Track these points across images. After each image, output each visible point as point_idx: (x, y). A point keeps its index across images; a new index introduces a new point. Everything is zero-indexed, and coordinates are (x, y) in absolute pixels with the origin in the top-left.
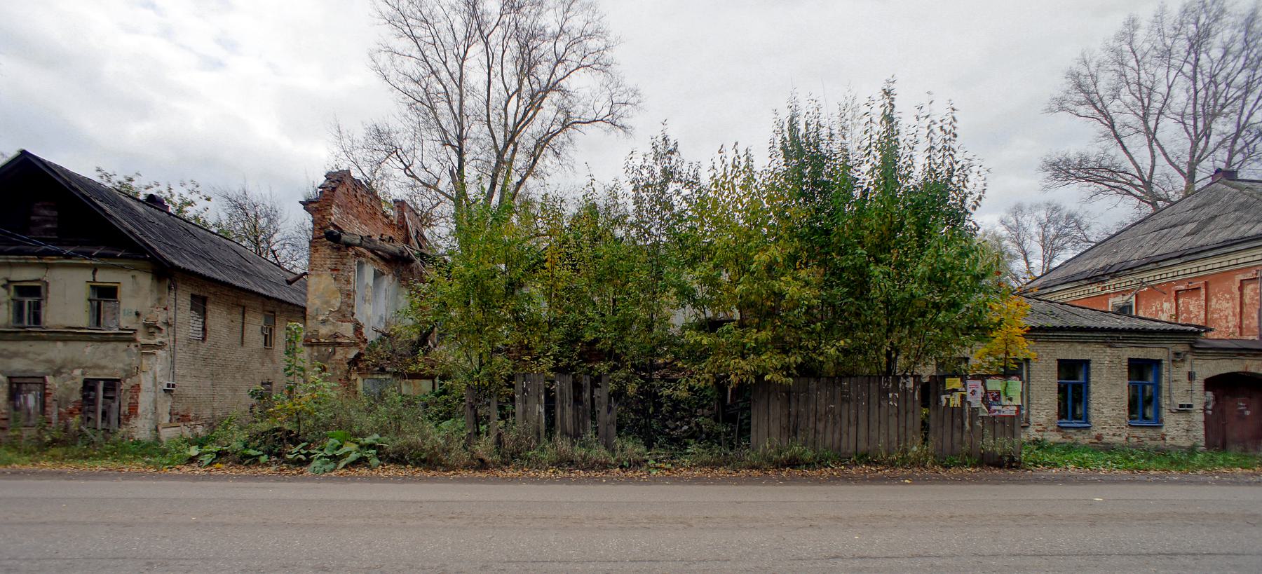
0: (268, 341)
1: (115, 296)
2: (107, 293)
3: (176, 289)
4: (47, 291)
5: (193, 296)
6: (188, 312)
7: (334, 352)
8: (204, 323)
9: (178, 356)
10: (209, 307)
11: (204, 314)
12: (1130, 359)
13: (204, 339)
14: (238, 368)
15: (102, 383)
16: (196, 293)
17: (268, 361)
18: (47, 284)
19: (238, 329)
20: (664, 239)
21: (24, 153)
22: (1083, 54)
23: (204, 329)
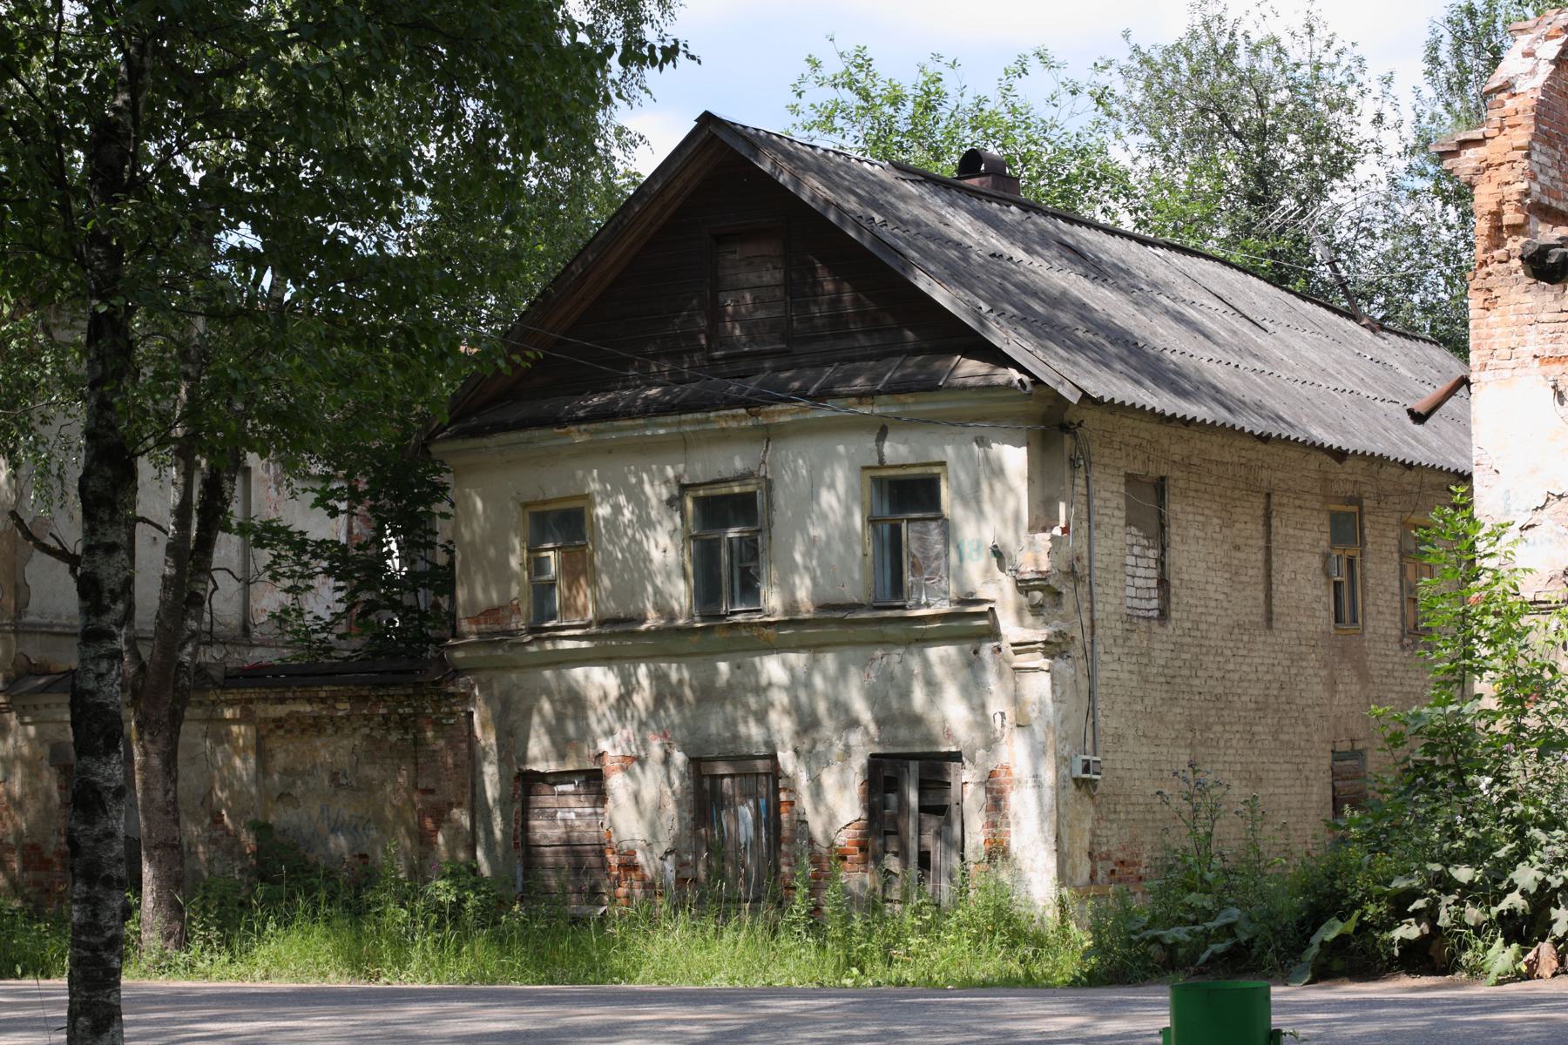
0: (1345, 604)
1: (934, 502)
2: (908, 497)
3: (1089, 464)
4: (770, 504)
5: (1131, 479)
6: (1120, 533)
7: (1383, 319)
8: (1161, 562)
9: (1102, 675)
10: (1174, 507)
11: (1160, 535)
12: (707, 119)
13: (1164, 615)
14: (1261, 707)
15: (914, 766)
16: (1137, 468)
17: (1347, 674)
18: (769, 485)
19: (1256, 573)
20: (1292, 138)
21: (707, 119)
22: (313, 506)
23: (1163, 583)
